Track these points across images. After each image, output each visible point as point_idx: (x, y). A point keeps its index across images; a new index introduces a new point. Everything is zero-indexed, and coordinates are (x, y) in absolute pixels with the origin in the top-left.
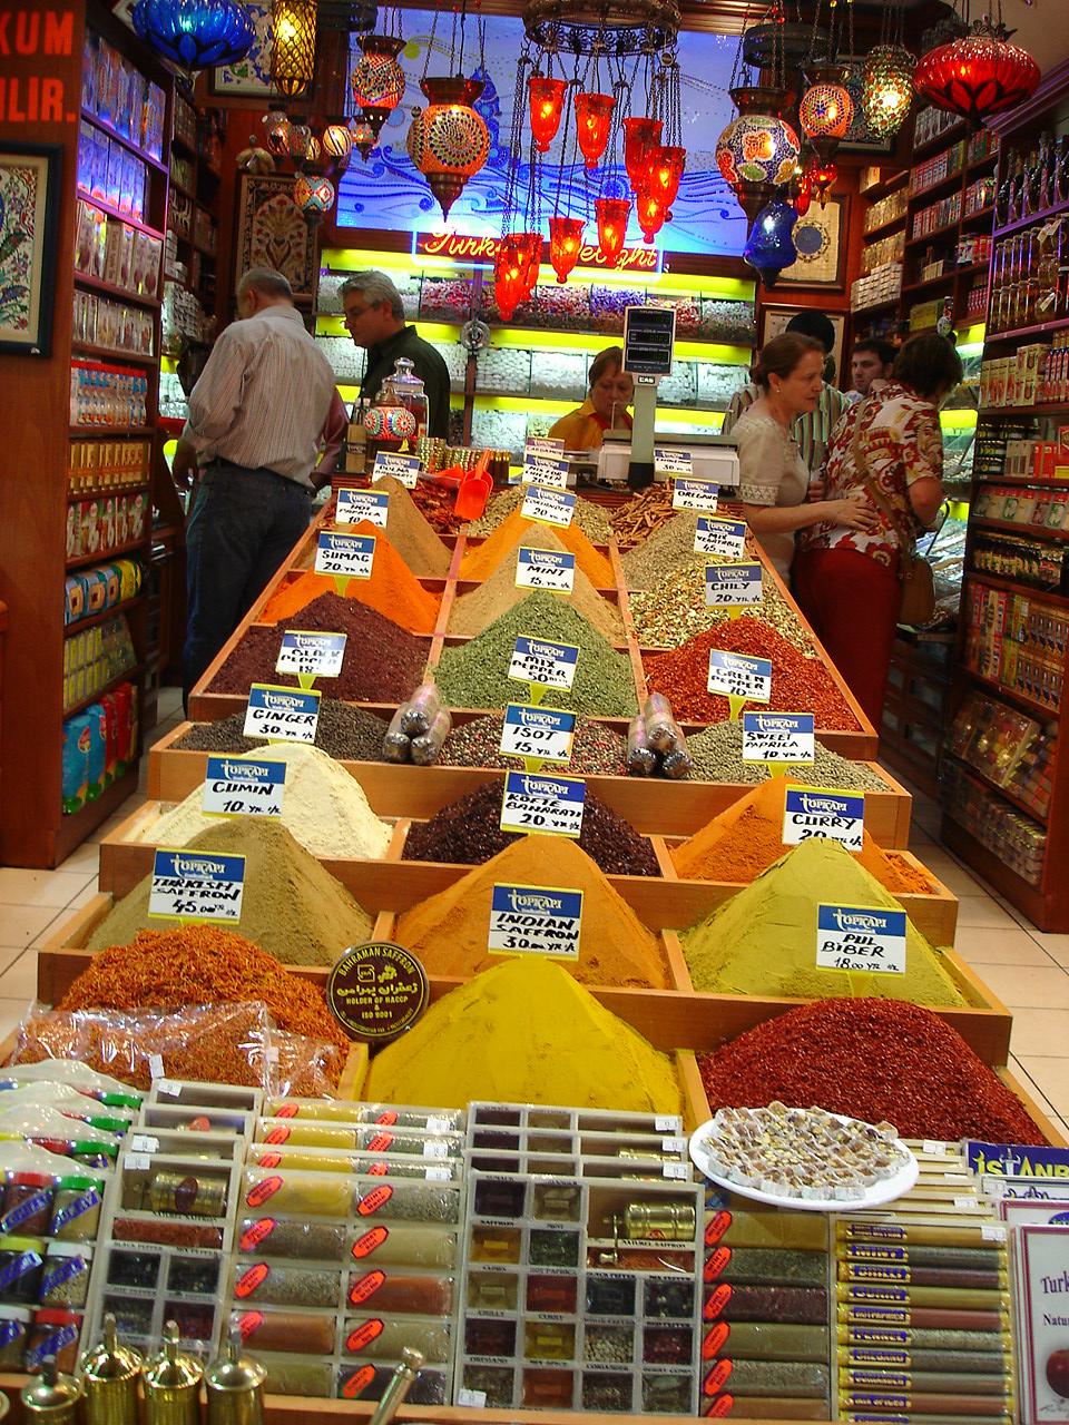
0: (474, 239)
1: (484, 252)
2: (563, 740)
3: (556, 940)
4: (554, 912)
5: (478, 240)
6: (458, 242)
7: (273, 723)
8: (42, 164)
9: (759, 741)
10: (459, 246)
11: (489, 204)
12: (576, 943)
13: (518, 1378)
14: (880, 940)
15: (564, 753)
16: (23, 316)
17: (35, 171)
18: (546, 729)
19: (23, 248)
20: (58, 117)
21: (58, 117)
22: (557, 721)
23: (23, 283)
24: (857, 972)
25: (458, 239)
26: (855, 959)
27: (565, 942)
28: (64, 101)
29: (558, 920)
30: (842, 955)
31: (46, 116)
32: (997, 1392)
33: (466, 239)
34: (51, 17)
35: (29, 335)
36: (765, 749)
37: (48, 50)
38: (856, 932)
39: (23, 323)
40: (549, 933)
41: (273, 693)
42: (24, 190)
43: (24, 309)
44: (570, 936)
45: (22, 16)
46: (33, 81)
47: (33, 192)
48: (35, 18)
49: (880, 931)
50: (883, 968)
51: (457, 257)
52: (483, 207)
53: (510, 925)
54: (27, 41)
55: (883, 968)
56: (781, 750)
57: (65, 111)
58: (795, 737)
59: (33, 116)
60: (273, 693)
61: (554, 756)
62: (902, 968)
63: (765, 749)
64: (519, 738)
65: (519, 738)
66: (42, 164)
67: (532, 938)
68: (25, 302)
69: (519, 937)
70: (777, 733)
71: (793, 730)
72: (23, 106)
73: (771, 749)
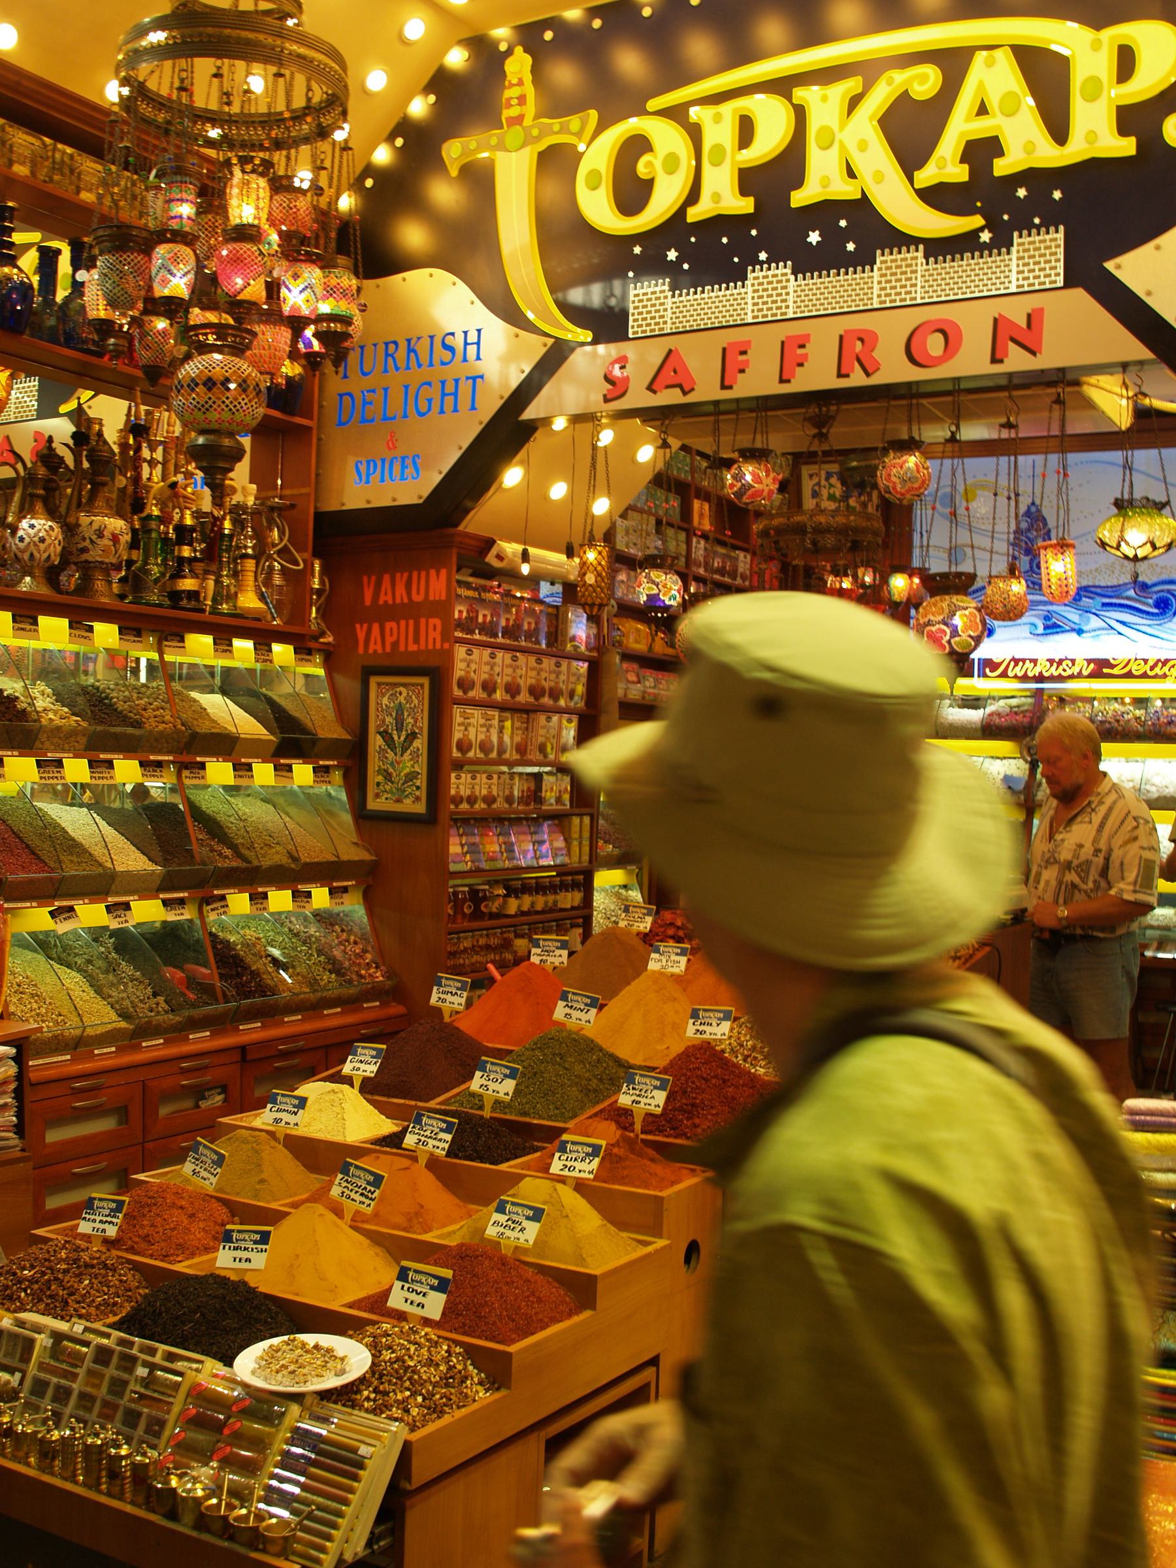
0: (1031, 661)
1: (1041, 673)
2: (509, 1085)
3: (363, 1199)
4: (369, 1183)
5: (1034, 661)
6: (1016, 665)
7: (358, 1065)
8: (426, 681)
9: (631, 1092)
10: (1018, 668)
11: (1046, 627)
12: (373, 1203)
13: (107, 1380)
14: (526, 1223)
15: (507, 1094)
16: (418, 793)
17: (422, 686)
18: (500, 1076)
19: (417, 743)
20: (438, 646)
21: (438, 646)
22: (508, 1072)
23: (417, 769)
24: (507, 1242)
25: (1016, 661)
26: (508, 1233)
27: (367, 1201)
28: (442, 634)
29: (369, 1188)
30: (502, 1229)
31: (431, 647)
32: (356, 1478)
33: (1024, 661)
34: (433, 572)
35: (421, 808)
36: (634, 1097)
37: (431, 598)
38: (515, 1217)
39: (418, 799)
40: (362, 1194)
41: (492, 1063)
42: (416, 701)
43: (418, 788)
44: (371, 1199)
45: (415, 574)
46: (423, 621)
47: (421, 702)
48: (423, 574)
49: (528, 1218)
50: (522, 1241)
51: (1025, 678)
52: (1040, 630)
53: (344, 1184)
54: (418, 593)
55: (522, 1241)
56: (643, 1100)
57: (442, 642)
58: (656, 1093)
59: (423, 647)
60: (492, 1063)
61: (501, 1095)
62: (531, 1242)
63: (634, 1097)
64: (483, 1081)
65: (483, 1081)
66: (426, 681)
67: (353, 1195)
68: (418, 783)
69: (347, 1192)
70: (645, 1087)
71: (656, 1088)
72: (416, 640)
73: (638, 1099)
